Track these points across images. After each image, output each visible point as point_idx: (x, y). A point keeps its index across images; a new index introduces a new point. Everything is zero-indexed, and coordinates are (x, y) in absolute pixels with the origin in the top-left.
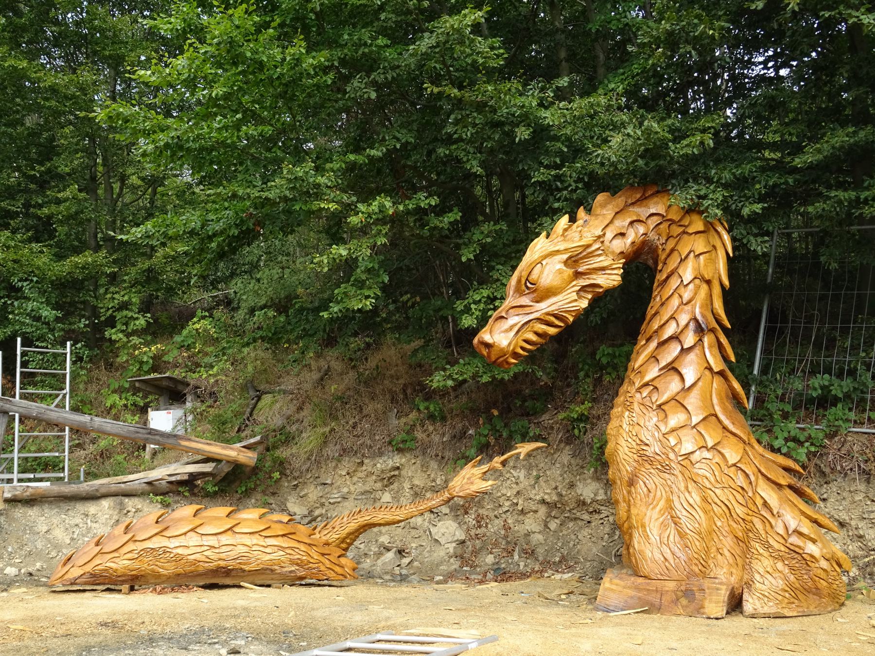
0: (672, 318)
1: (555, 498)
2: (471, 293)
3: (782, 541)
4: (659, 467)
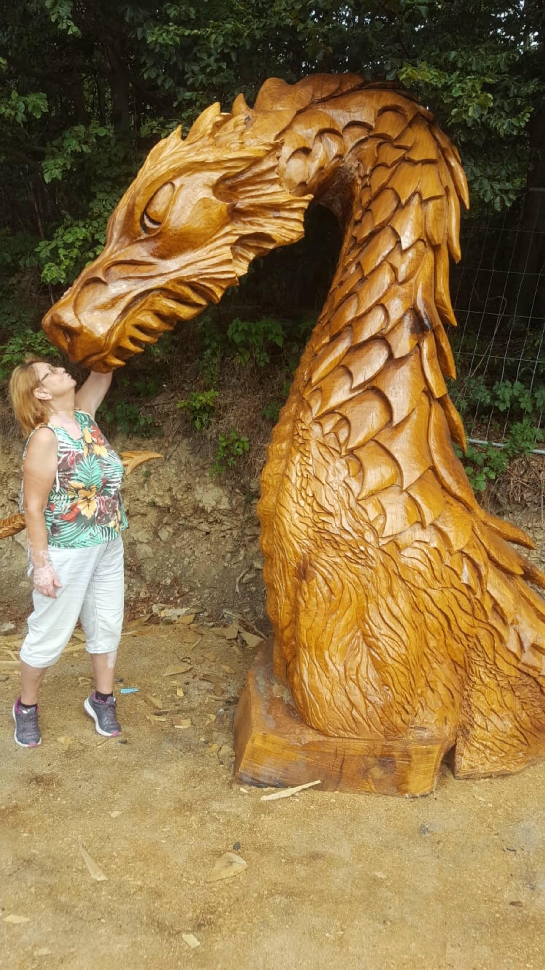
0: (380, 304)
1: (168, 501)
2: (60, 231)
3: (514, 661)
4: (349, 554)
